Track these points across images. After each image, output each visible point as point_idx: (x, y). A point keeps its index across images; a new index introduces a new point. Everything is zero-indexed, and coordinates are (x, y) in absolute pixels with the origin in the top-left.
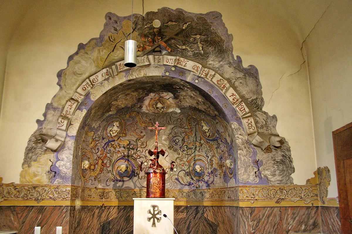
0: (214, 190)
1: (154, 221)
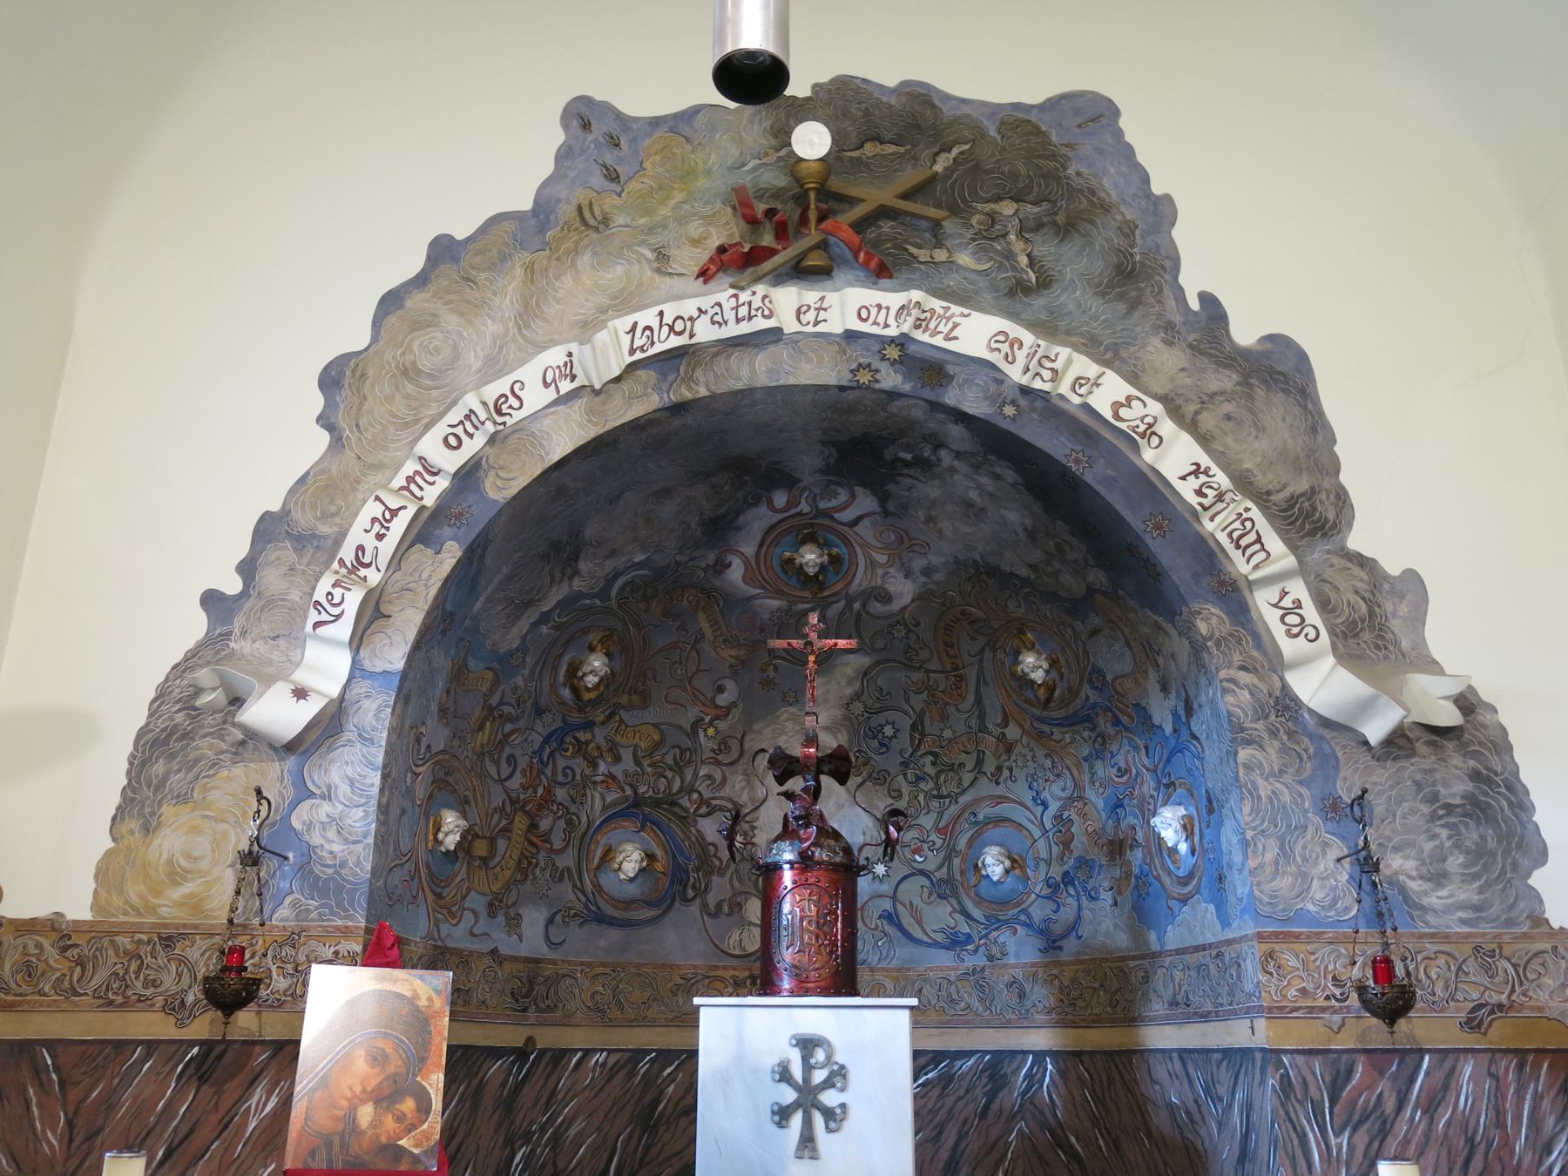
0: (1082, 967)
1: (808, 1123)
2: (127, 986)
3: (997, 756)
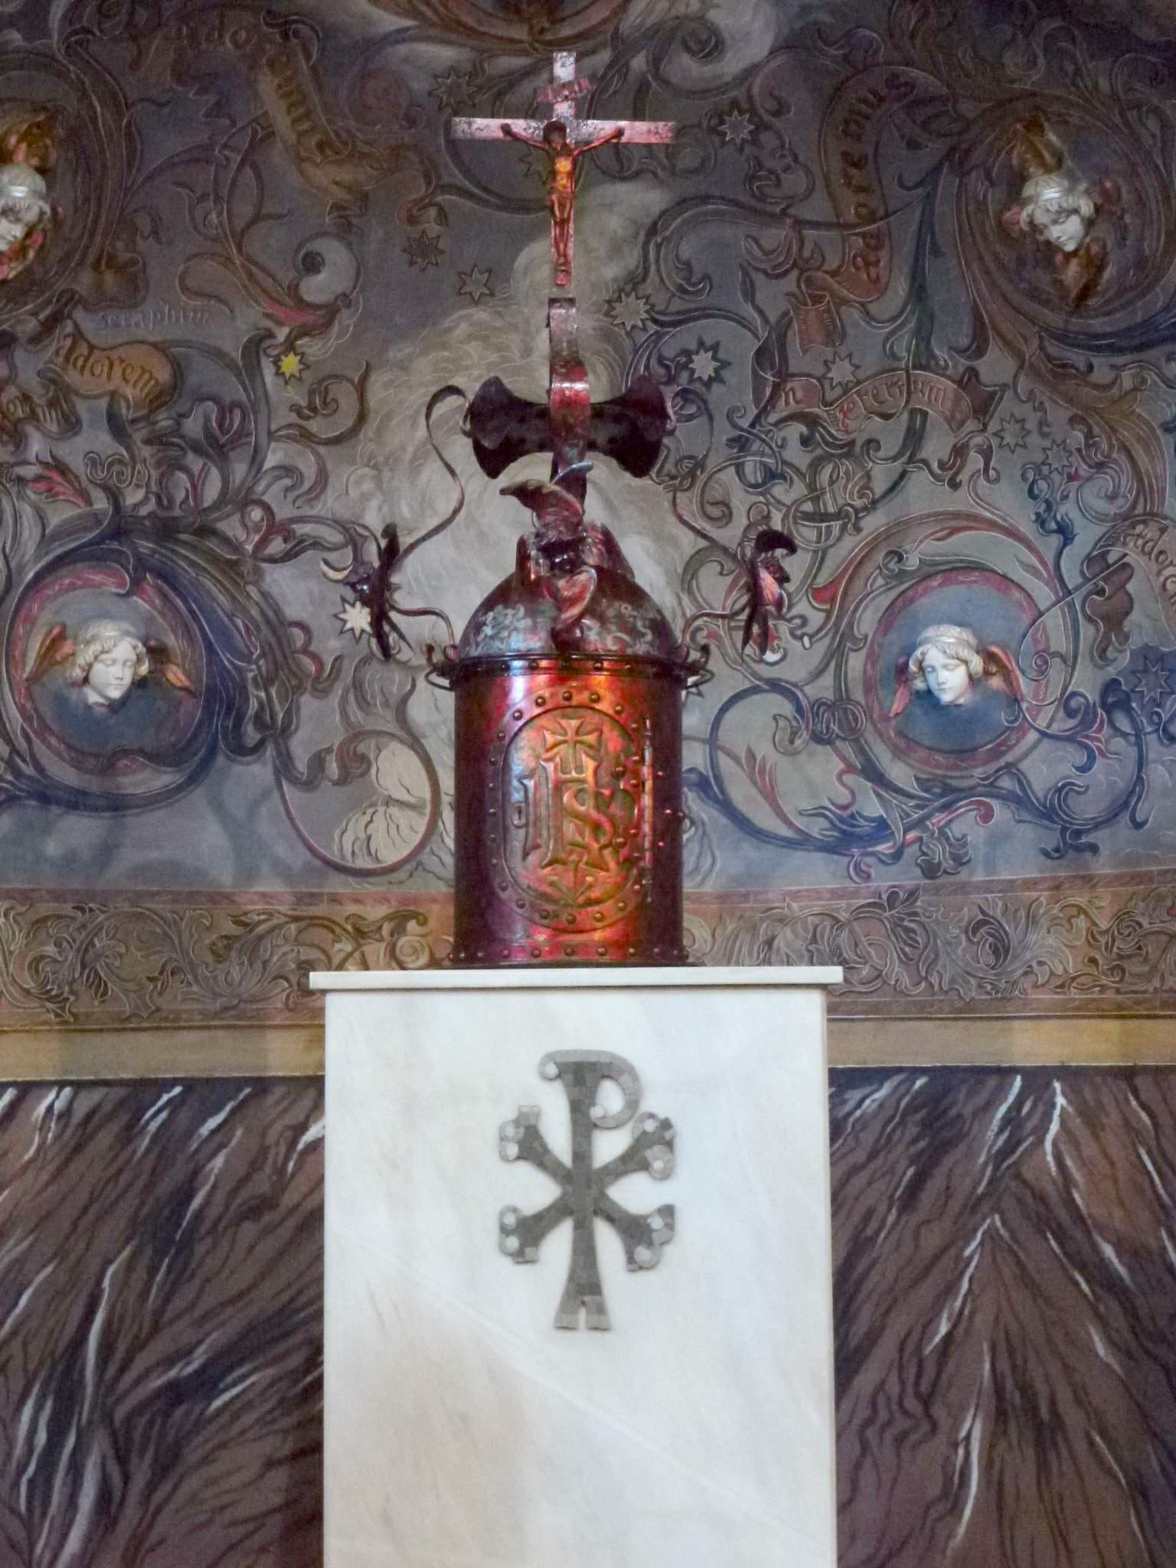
1: (585, 1252)
3: (954, 423)
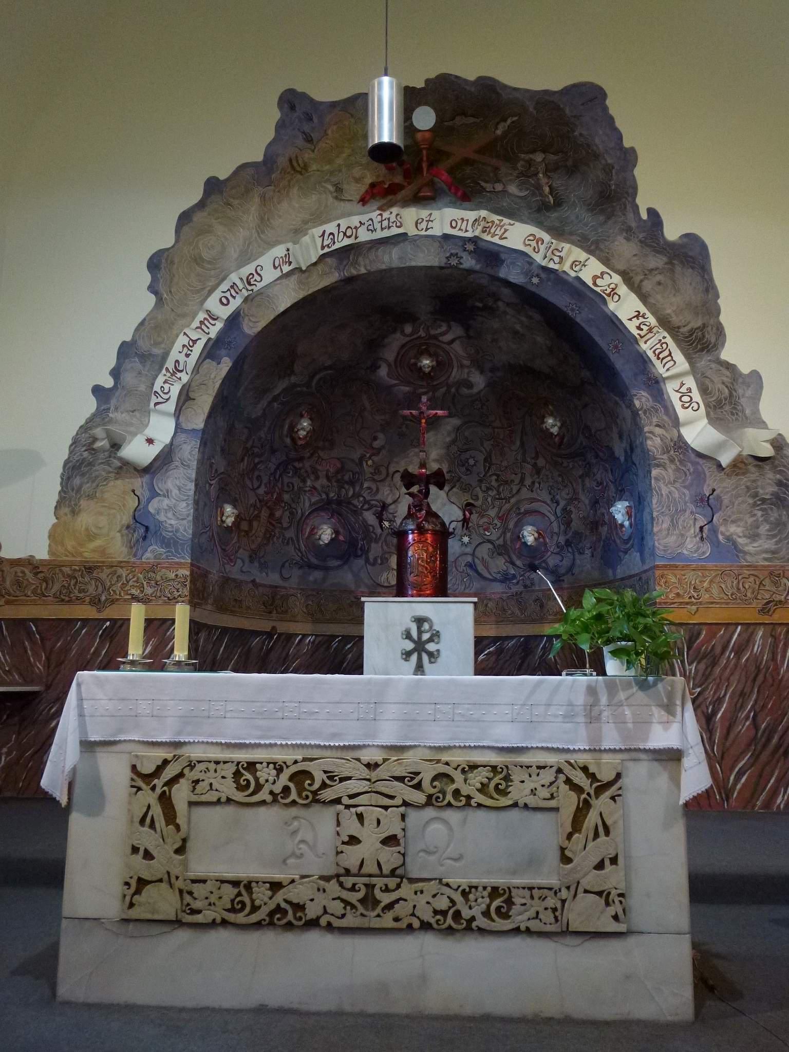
1: (420, 659)
2: (70, 592)
3: (532, 476)
